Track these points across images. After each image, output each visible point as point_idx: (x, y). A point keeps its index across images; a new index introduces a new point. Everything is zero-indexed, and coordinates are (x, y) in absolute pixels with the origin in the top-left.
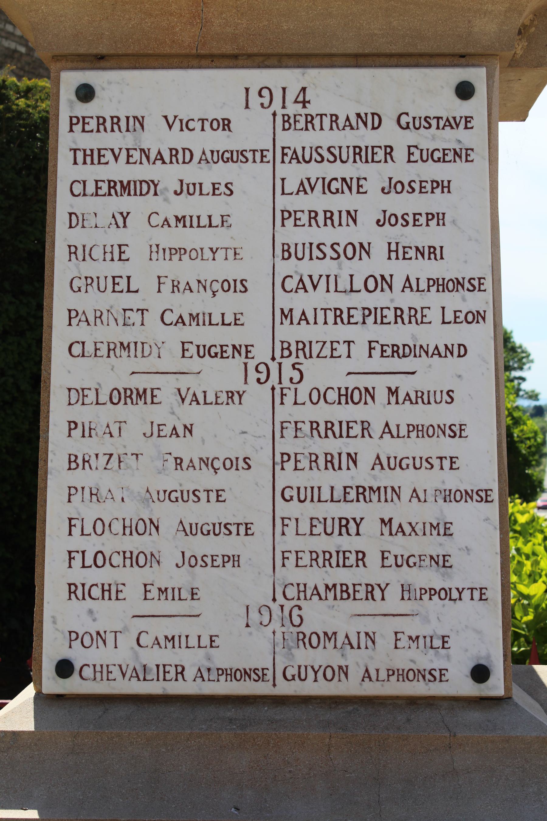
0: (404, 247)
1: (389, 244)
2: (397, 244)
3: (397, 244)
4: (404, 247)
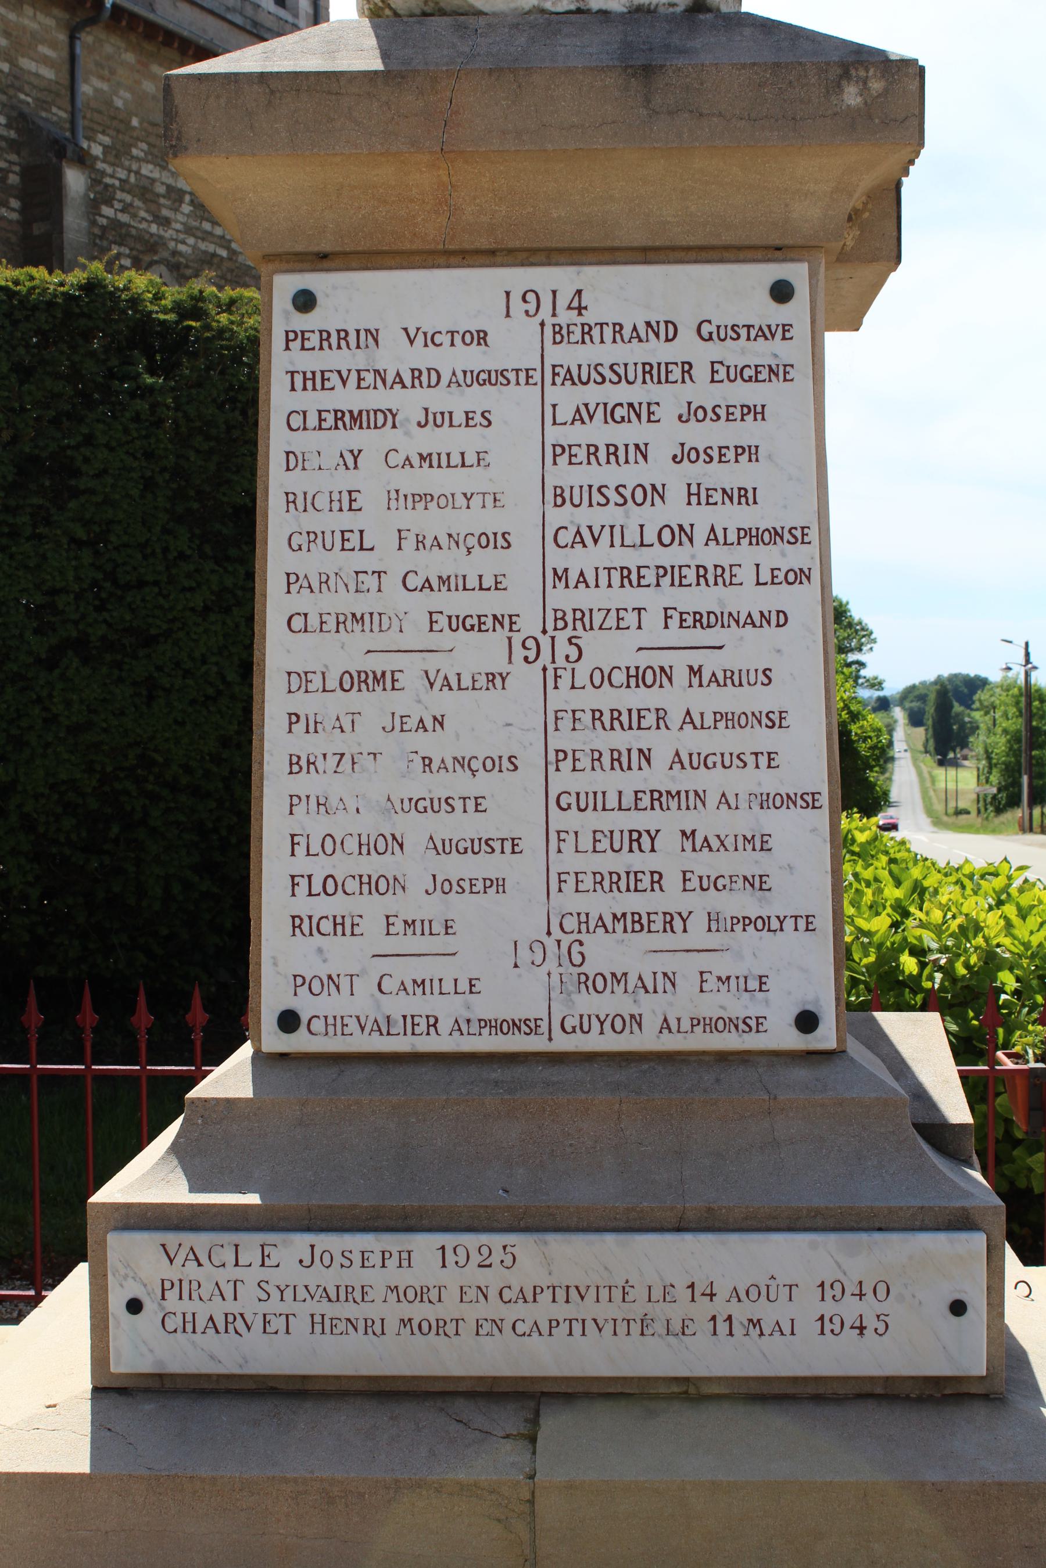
0: (708, 490)
1: (689, 485)
2: (699, 485)
3: (699, 485)
4: (708, 490)
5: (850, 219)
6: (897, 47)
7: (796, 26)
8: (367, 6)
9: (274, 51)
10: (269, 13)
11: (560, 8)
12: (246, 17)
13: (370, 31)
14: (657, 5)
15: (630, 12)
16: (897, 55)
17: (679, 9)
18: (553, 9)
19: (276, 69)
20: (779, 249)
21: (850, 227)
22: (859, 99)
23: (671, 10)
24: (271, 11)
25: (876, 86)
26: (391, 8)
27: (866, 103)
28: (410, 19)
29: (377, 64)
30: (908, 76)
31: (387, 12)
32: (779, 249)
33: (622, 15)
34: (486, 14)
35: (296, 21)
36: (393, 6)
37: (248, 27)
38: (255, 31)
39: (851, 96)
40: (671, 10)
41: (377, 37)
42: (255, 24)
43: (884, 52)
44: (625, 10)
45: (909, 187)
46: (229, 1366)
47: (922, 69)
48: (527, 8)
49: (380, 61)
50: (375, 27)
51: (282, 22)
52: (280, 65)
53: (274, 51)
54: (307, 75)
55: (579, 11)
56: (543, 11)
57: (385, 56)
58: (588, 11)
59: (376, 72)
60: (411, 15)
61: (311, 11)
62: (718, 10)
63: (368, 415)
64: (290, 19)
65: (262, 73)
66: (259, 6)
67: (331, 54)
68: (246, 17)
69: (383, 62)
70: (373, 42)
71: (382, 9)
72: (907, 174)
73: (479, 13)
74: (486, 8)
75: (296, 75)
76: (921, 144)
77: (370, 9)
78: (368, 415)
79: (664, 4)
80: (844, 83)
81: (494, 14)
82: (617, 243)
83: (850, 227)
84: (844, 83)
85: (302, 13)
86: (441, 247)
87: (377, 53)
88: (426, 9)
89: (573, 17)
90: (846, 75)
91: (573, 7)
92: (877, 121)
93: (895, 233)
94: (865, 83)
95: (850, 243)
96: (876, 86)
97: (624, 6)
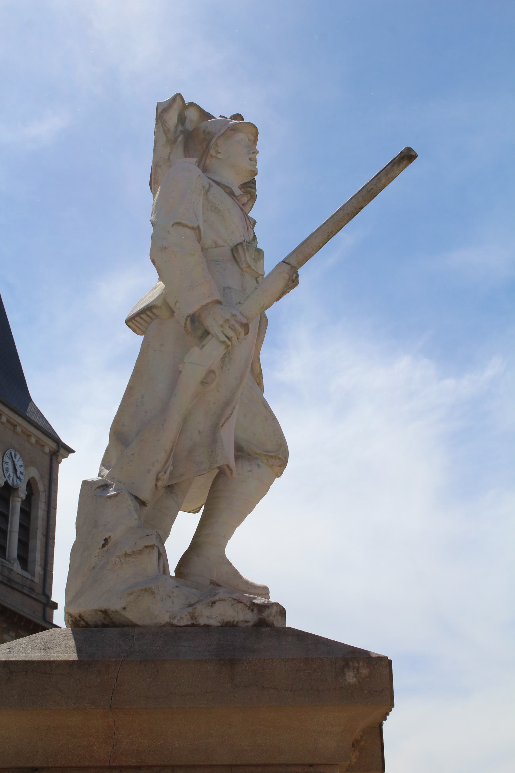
5: (353, 746)
6: (375, 648)
7: (317, 636)
8: (70, 619)
9: (14, 647)
10: (18, 574)
11: (182, 624)
12: (4, 576)
13: (71, 636)
14: (238, 622)
15: (222, 626)
16: (375, 654)
17: (250, 624)
18: (178, 624)
19: (14, 659)
20: (311, 765)
21: (354, 751)
22: (355, 679)
23: (246, 624)
24: (19, 573)
25: (364, 672)
26: (84, 621)
27: (359, 681)
28: (95, 629)
29: (73, 656)
30: (383, 665)
31: (82, 623)
32: (311, 765)
33: (218, 627)
34: (139, 626)
35: (33, 578)
36: (86, 620)
37: (5, 582)
38: (9, 584)
39: (350, 677)
40: (246, 624)
41: (75, 639)
42: (9, 580)
43: (368, 652)
44: (219, 625)
45: (386, 726)
46: (24, 421)
47: (390, 662)
48: (163, 623)
49: (76, 655)
50: (74, 633)
51: (24, 579)
52: (17, 657)
53: (14, 647)
54: (33, 662)
55: (193, 625)
56: (172, 625)
57: (79, 651)
58: (198, 626)
59: (73, 662)
60: (96, 626)
61: (42, 573)
62: (273, 624)
63: (147, 322)
64: (29, 577)
65: (6, 661)
66: (12, 570)
67: (48, 650)
68: (4, 576)
69: (78, 656)
70: (72, 642)
71: (79, 621)
72: (385, 720)
73: (135, 626)
74: (139, 623)
75: (26, 662)
76: (393, 705)
77: (72, 620)
78: (147, 322)
79: (242, 621)
80: (346, 670)
81: (144, 627)
82: (214, 763)
83: (354, 751)
84: (346, 670)
85: (37, 574)
86: (107, 764)
87: (74, 649)
88: (104, 622)
89: (189, 629)
90: (346, 665)
91: (189, 623)
92: (366, 692)
93: (380, 754)
94: (358, 670)
95: (354, 760)
96: (364, 672)
97: (219, 622)
